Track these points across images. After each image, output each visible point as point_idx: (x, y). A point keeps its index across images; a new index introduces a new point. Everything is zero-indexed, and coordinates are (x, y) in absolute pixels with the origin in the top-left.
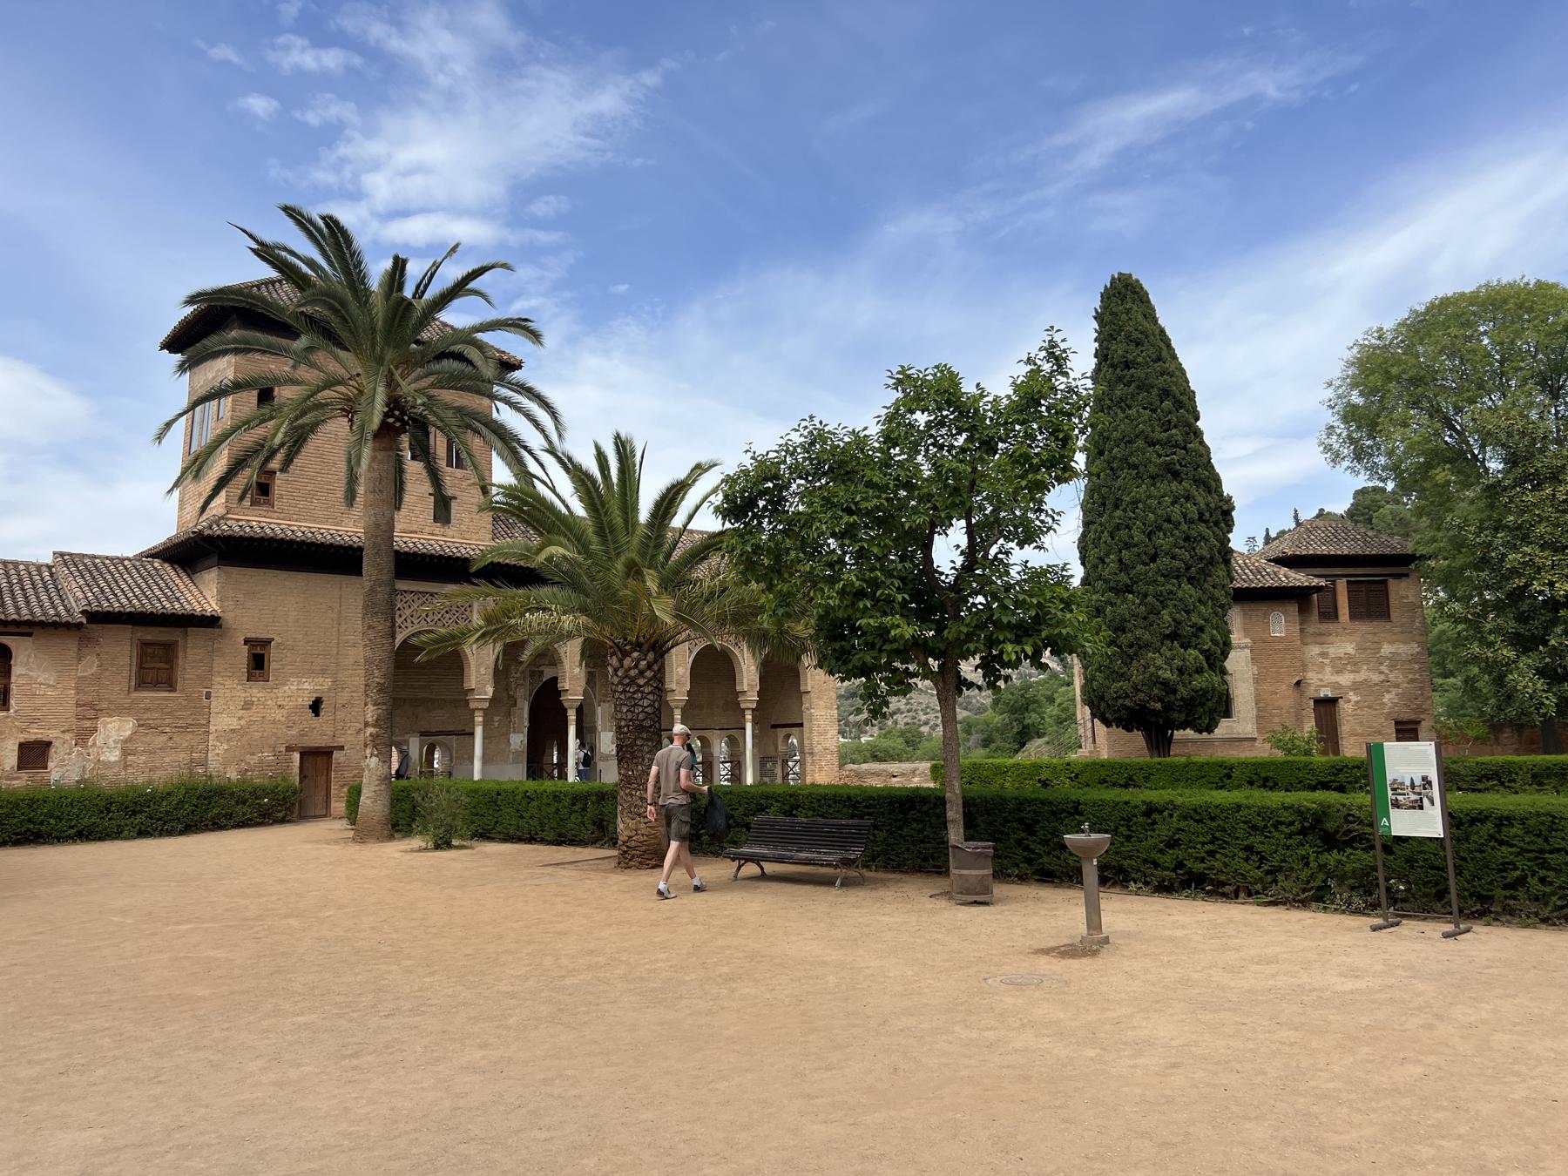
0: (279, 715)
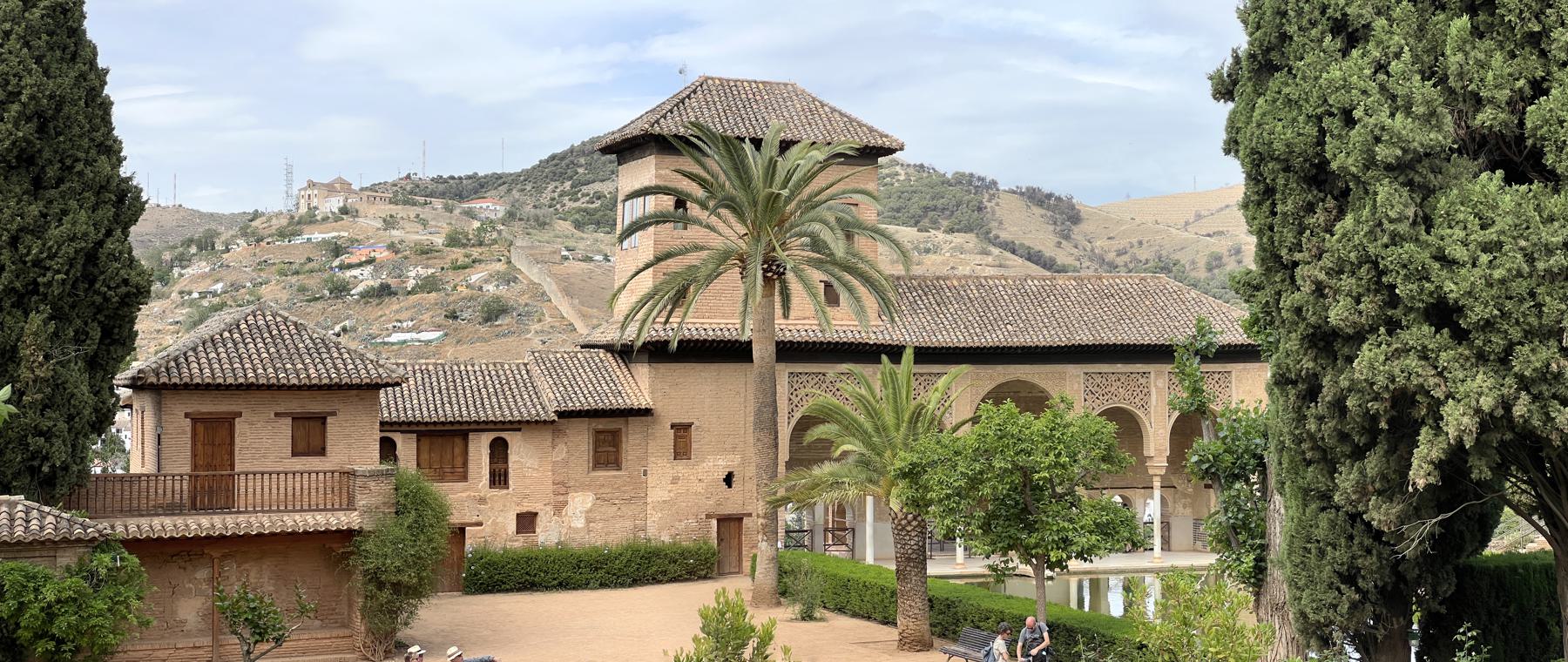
0: (700, 488)
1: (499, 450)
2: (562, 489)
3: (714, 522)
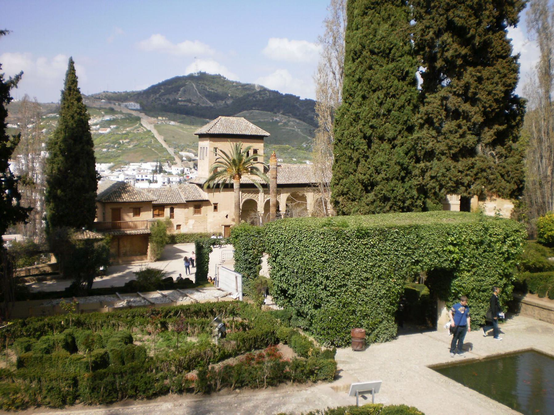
1: (172, 211)
2: (187, 219)
3: (223, 227)
